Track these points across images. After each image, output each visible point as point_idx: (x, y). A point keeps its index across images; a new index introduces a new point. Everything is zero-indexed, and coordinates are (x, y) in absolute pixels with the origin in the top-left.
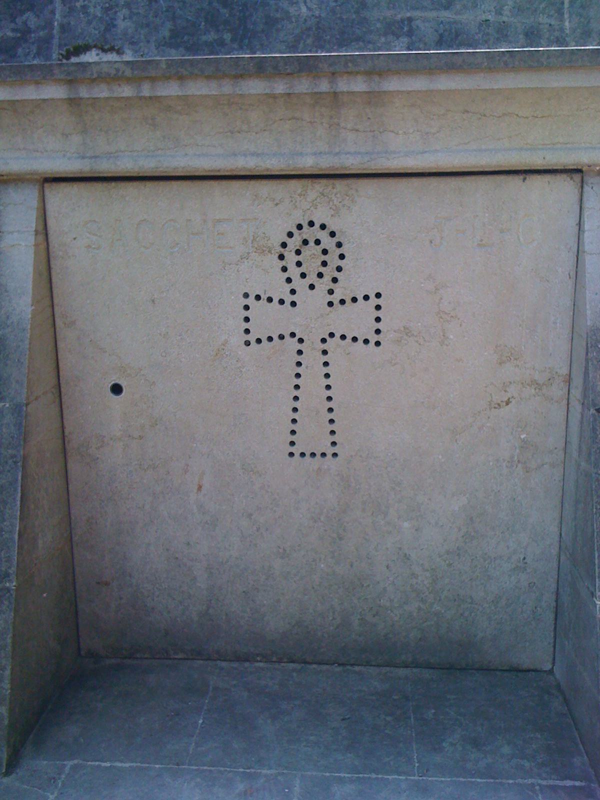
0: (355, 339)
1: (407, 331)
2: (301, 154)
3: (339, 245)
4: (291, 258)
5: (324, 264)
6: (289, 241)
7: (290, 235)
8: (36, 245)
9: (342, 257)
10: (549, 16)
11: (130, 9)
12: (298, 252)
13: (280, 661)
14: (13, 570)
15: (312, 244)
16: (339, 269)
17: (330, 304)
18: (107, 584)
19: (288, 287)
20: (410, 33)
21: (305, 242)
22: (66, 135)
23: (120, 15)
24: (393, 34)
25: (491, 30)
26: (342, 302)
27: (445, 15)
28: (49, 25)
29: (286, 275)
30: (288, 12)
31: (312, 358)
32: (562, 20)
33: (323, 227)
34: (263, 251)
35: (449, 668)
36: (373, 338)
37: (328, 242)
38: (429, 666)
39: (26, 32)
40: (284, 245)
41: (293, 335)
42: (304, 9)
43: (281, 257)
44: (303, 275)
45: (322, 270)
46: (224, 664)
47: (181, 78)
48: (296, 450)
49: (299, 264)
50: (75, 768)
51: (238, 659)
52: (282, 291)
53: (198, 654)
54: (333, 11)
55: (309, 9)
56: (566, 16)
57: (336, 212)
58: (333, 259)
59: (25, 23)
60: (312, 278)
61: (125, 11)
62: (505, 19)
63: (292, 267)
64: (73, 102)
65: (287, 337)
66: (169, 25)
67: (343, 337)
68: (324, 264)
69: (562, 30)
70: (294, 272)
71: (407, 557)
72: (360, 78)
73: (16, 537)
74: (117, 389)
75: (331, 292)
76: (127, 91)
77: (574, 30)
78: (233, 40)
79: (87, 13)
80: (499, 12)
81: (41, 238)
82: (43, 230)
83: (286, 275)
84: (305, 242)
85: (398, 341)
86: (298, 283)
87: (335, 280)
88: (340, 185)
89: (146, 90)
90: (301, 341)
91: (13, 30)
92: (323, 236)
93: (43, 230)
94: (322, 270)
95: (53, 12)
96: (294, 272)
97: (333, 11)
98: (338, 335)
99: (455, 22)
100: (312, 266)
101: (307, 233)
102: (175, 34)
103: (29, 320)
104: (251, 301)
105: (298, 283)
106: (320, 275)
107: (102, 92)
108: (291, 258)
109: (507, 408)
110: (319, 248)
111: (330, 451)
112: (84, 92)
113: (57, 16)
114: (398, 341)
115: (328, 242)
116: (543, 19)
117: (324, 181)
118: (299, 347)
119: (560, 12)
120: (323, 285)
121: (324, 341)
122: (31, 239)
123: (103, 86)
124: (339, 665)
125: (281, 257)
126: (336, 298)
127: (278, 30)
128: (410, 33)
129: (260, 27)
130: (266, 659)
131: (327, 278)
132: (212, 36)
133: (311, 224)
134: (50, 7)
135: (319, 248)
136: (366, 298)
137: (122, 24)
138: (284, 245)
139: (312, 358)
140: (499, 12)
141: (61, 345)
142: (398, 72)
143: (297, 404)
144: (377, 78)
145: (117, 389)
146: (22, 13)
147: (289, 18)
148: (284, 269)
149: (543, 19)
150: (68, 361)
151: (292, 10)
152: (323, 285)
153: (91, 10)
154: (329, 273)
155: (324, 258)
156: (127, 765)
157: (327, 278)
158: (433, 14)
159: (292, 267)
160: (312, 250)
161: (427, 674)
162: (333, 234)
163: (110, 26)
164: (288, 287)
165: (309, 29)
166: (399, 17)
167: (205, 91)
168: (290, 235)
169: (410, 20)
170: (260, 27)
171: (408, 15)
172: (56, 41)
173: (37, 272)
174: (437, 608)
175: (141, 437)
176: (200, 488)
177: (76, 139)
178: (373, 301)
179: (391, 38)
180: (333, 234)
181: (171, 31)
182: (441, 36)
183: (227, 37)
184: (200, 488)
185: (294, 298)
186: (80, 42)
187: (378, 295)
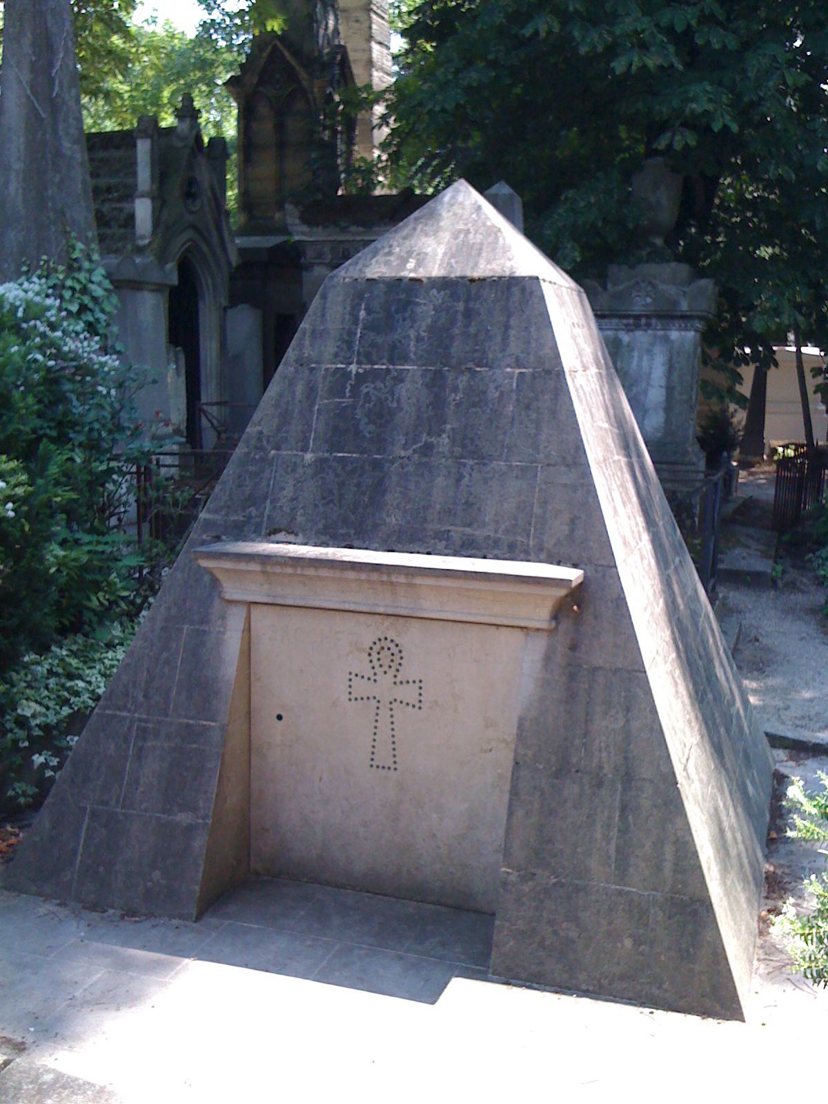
0: (408, 704)
1: (436, 702)
2: (377, 605)
3: (400, 651)
4: (375, 656)
5: (392, 661)
6: (374, 647)
7: (375, 643)
8: (242, 638)
9: (402, 658)
10: (523, 537)
11: (304, 510)
12: (379, 653)
13: (360, 891)
14: (211, 814)
15: (386, 649)
16: (400, 664)
17: (395, 683)
18: (267, 830)
19: (372, 671)
20: (447, 539)
21: (383, 648)
22: (262, 585)
23: (299, 513)
24: (439, 539)
25: (490, 542)
26: (401, 683)
27: (468, 530)
28: (262, 515)
29: (372, 665)
30: (385, 520)
31: (385, 713)
32: (529, 540)
33: (392, 641)
34: (360, 650)
35: (458, 908)
36: (417, 705)
37: (394, 650)
38: (447, 906)
39: (250, 518)
40: (371, 648)
41: (374, 698)
42: (394, 519)
43: (370, 655)
44: (381, 666)
45: (391, 664)
46: (329, 888)
47: (316, 568)
48: (374, 763)
49: (379, 659)
50: (229, 924)
51: (337, 886)
52: (370, 673)
53: (315, 880)
54: (408, 522)
55: (396, 520)
56: (531, 538)
57: (399, 634)
58: (397, 658)
59: (250, 513)
60: (385, 668)
61: (302, 511)
62: (499, 536)
63: (375, 661)
64: (264, 572)
65: (371, 699)
66: (323, 521)
67: (401, 702)
68: (392, 661)
69: (528, 545)
70: (376, 663)
71: (434, 835)
72: (402, 576)
73: (214, 797)
74: (280, 717)
75: (395, 676)
76: (290, 570)
77: (534, 546)
78: (355, 533)
79: (282, 511)
80: (496, 531)
81: (246, 633)
82: (248, 629)
83: (372, 665)
84: (383, 648)
85: (431, 708)
86: (377, 669)
87: (398, 670)
88: (401, 620)
89: (299, 571)
90: (379, 701)
91: (244, 516)
92: (392, 646)
93: (248, 629)
94: (391, 664)
95: (265, 507)
96: (376, 663)
97: (408, 522)
98: (398, 701)
99: (473, 535)
100: (386, 662)
101: (383, 643)
102: (326, 527)
103: (110, 972)
104: (353, 677)
105: (377, 669)
106: (390, 667)
107: (278, 570)
108: (375, 656)
109: (491, 753)
110: (389, 653)
111: (393, 766)
112: (269, 569)
113: (267, 510)
114: (431, 708)
115: (394, 650)
116: (519, 538)
117: (393, 618)
118: (377, 705)
119: (528, 535)
120: (391, 672)
121: (391, 703)
122: (240, 635)
123: (279, 567)
124: (395, 897)
125: (370, 655)
126: (398, 680)
127: (379, 531)
128: (447, 539)
129: (370, 528)
130: (354, 888)
131: (393, 669)
132: (343, 531)
133: (386, 639)
134: (263, 505)
135: (389, 653)
136: (414, 682)
137: (299, 519)
138: (371, 648)
139: (385, 713)
140: (496, 531)
141: (252, 690)
142: (420, 575)
143: (375, 737)
144: (411, 577)
145: (280, 717)
146: (249, 507)
147: (385, 524)
148: (371, 661)
149: (519, 538)
150: (254, 698)
151: (388, 520)
152: (391, 672)
153: (284, 509)
154: (395, 666)
155: (392, 657)
156: (256, 926)
157: (393, 669)
158: (461, 529)
159: (375, 661)
160: (385, 653)
161: (444, 910)
162: (397, 645)
163: (293, 519)
164: (372, 671)
165: (395, 531)
166: (442, 529)
167: (326, 574)
168: (375, 643)
169: (449, 531)
170: (370, 528)
171: (448, 528)
172: (264, 525)
173: (242, 652)
174: (451, 869)
175: (291, 746)
176: (321, 780)
177: (266, 586)
178: (418, 684)
179: (437, 541)
180: (397, 645)
181: (324, 525)
182: (464, 542)
183: (352, 532)
184: (321, 780)
185: (376, 677)
186: (277, 527)
187: (421, 681)
